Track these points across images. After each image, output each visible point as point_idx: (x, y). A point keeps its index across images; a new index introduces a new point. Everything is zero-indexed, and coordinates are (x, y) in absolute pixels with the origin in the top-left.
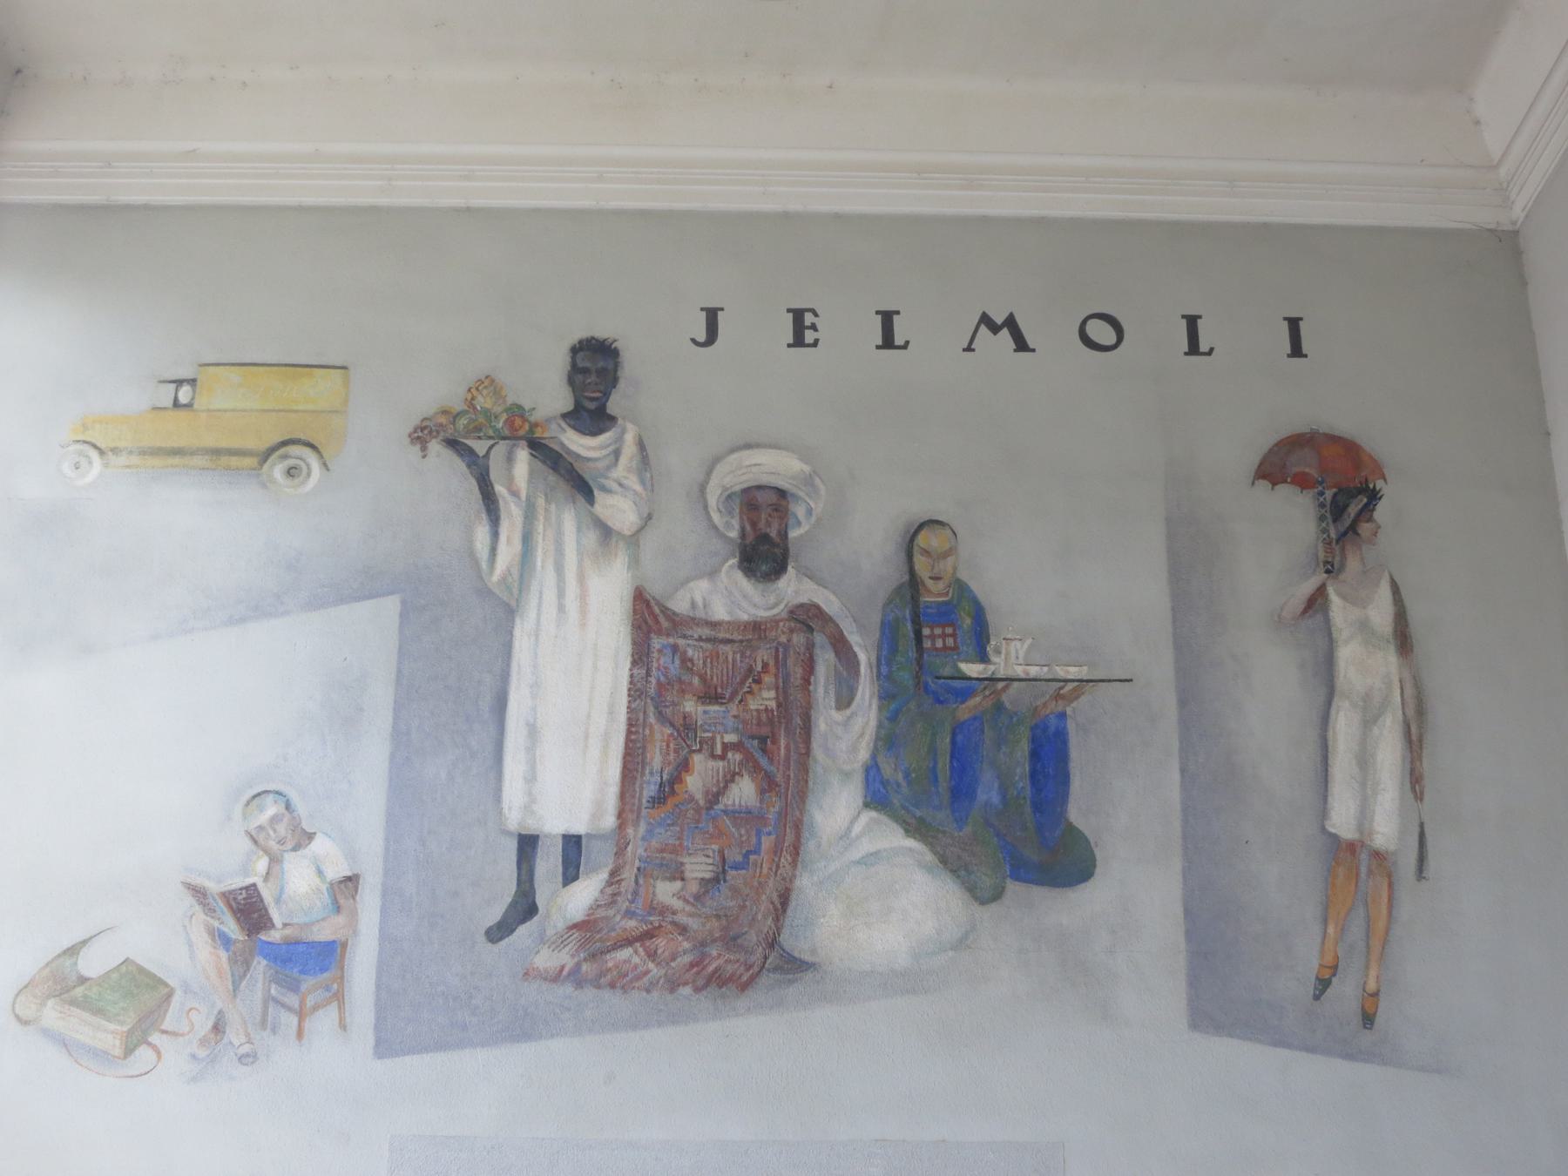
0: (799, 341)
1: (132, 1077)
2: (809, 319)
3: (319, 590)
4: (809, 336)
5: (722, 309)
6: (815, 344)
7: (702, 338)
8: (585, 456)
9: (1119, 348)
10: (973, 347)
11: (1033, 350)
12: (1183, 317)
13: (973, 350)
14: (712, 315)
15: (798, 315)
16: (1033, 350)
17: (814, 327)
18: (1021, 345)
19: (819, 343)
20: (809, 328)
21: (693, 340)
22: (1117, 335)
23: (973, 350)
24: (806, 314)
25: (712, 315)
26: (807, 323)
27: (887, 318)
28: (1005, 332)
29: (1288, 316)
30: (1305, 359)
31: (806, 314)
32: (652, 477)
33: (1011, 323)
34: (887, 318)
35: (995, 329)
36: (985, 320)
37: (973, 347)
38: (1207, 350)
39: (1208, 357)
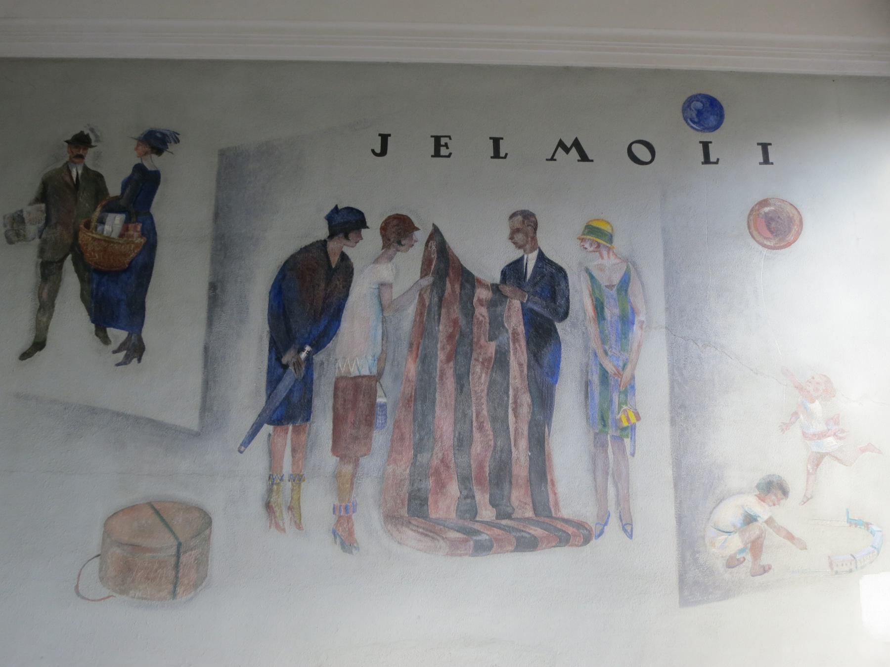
0: (437, 154)
1: (104, 599)
2: (443, 141)
3: (73, 221)
4: (444, 151)
5: (502, 139)
6: (449, 156)
7: (378, 150)
8: (93, 169)
9: (655, 160)
10: (555, 158)
11: (592, 161)
12: (491, 138)
13: (555, 160)
14: (384, 138)
15: (437, 139)
16: (592, 161)
17: (446, 145)
18: (584, 157)
19: (508, 156)
20: (443, 146)
21: (373, 151)
22: (652, 154)
23: (555, 160)
24: (442, 138)
25: (384, 138)
26: (442, 143)
27: (496, 142)
28: (574, 151)
29: (702, 140)
30: (555, 162)
31: (442, 138)
32: (527, 258)
33: (577, 144)
34: (496, 142)
35: (567, 150)
36: (561, 144)
37: (555, 158)
38: (715, 160)
39: (448, 158)
